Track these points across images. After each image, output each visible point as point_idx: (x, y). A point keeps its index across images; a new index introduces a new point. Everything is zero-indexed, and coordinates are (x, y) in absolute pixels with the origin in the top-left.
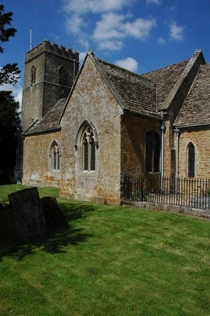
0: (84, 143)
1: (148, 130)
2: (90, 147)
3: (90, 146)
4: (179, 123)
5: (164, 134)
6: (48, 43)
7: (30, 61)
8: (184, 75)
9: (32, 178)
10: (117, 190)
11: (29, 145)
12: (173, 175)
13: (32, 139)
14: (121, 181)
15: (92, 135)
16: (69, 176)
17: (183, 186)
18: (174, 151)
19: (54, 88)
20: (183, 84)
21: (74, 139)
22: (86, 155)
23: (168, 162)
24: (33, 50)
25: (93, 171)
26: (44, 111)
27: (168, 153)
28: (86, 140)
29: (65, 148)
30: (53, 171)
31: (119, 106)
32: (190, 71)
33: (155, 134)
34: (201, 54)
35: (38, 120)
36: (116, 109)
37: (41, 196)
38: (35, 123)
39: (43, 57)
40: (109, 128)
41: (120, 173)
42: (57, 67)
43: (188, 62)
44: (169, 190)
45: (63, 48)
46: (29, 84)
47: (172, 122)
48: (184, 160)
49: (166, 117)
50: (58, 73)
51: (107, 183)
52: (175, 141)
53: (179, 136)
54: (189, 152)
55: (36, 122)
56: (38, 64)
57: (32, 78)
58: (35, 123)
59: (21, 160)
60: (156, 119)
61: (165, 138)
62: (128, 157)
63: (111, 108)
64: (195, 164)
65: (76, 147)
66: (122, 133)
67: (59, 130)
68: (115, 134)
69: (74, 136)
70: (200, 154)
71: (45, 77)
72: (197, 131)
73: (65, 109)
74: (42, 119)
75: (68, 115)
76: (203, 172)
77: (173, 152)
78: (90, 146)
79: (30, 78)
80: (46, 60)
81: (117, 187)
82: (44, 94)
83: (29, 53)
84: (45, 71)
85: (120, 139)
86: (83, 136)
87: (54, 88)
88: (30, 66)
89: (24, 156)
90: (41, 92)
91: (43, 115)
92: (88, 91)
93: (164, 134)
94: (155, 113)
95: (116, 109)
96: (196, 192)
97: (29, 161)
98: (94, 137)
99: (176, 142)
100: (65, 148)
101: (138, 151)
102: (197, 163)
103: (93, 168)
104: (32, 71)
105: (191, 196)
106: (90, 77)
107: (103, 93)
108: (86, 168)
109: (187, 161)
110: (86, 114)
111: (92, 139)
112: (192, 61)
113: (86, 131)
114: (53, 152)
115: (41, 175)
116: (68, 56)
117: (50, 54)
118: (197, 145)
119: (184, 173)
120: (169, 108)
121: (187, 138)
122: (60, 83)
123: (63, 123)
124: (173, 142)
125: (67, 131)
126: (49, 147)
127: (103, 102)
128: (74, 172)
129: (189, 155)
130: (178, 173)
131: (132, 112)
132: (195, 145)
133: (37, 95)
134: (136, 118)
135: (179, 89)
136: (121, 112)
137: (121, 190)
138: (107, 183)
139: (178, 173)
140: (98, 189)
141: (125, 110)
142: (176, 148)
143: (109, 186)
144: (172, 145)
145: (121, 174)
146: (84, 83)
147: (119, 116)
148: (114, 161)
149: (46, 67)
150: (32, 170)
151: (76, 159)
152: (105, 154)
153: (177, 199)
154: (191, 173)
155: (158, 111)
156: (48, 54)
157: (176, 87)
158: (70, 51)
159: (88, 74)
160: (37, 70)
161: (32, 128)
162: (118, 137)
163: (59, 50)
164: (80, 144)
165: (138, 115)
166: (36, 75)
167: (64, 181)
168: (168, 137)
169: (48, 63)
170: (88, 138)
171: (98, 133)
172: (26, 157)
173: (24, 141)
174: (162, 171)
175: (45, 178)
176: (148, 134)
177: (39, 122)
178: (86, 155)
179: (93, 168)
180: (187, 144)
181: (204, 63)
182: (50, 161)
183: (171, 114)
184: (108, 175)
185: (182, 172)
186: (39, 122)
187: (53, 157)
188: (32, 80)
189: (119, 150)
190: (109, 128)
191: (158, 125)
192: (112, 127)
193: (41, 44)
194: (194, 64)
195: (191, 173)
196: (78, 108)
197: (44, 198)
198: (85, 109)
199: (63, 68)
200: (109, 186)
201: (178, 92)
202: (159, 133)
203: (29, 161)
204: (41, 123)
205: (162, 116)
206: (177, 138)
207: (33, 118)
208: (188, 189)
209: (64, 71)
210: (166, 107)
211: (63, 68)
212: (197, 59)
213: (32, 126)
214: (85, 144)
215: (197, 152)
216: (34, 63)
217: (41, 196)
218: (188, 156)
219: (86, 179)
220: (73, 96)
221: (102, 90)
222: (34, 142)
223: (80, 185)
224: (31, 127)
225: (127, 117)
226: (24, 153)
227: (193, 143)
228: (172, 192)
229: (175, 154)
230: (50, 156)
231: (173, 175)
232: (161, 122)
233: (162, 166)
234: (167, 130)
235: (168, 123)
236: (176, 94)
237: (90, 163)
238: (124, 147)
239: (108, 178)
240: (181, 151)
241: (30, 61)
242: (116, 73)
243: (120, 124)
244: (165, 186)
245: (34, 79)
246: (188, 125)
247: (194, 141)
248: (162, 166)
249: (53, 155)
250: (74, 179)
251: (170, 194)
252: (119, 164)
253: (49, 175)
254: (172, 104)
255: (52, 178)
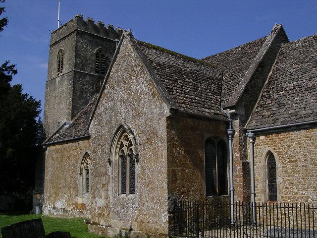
0: (121, 156)
1: (207, 136)
2: (129, 160)
3: (128, 160)
4: (252, 124)
5: (232, 140)
6: (80, 18)
7: (56, 43)
8: (259, 58)
9: (56, 206)
10: (164, 221)
11: (52, 155)
12: (247, 198)
13: (57, 151)
14: (169, 209)
15: (130, 145)
16: (101, 202)
17: (261, 214)
18: (248, 163)
19: (88, 78)
20: (257, 70)
21: (107, 150)
22: (124, 173)
23: (239, 180)
24: (61, 28)
25: (132, 196)
26: (74, 113)
27: (239, 167)
28: (123, 151)
29: (96, 164)
30: (84, 196)
31: (164, 105)
32: (266, 53)
33: (220, 141)
34: (282, 29)
35: (65, 124)
36: (161, 108)
37: (48, 231)
38: (61, 128)
39: (74, 36)
40: (152, 135)
41: (167, 197)
42: (93, 49)
43: (265, 40)
44: (242, 221)
45: (102, 25)
46: (54, 74)
47: (243, 123)
48: (262, 176)
49: (234, 116)
50: (94, 58)
51: (151, 211)
52: (249, 151)
53: (253, 143)
54: (268, 165)
55: (63, 126)
56: (68, 47)
57: (59, 65)
58: (61, 128)
59: (42, 179)
60: (219, 121)
61: (233, 145)
62: (179, 174)
63: (153, 107)
64: (278, 181)
65: (110, 161)
66: (168, 142)
67: (88, 138)
68: (159, 143)
69: (107, 147)
70: (283, 167)
71: (76, 65)
72: (277, 133)
73: (95, 109)
74: (72, 122)
75: (99, 118)
76: (289, 193)
77: (246, 166)
78: (128, 160)
79: (56, 66)
80: (77, 41)
81: (165, 217)
82: (74, 88)
83: (55, 32)
84: (77, 56)
85: (166, 151)
86: (119, 147)
87: (88, 78)
88: (56, 49)
89: (46, 175)
90: (69, 85)
91: (73, 117)
92: (125, 84)
93: (232, 140)
94: (218, 112)
95: (161, 108)
96: (280, 221)
97: (52, 182)
98: (133, 147)
99: (250, 151)
100: (96, 164)
101: (196, 163)
102: (279, 180)
103: (132, 191)
104: (59, 57)
105: (303, 223)
106: (127, 65)
107: (143, 87)
108: (123, 192)
109: (266, 178)
110: (124, 115)
111: (131, 150)
112: (270, 39)
113: (122, 139)
114: (84, 168)
115: (69, 201)
116: (108, 35)
117: (83, 33)
118: (278, 155)
119: (263, 195)
120: (237, 104)
121: (263, 145)
122: (97, 72)
123: (93, 128)
124: (246, 151)
125: (98, 140)
126: (80, 161)
127: (144, 100)
128: (107, 198)
129: (269, 169)
130: (255, 194)
131: (183, 113)
132: (275, 155)
133: (64, 89)
134: (189, 120)
135: (252, 78)
136: (167, 112)
137: (169, 222)
138: (151, 211)
139: (255, 194)
140: (139, 220)
141: (171, 110)
142: (250, 160)
143: (154, 216)
144: (244, 156)
145: (169, 198)
146: (119, 74)
147: (165, 118)
148: (159, 181)
149: (77, 50)
150: (57, 194)
151: (109, 178)
152: (147, 171)
153: (244, 232)
154: (273, 196)
155: (224, 109)
156: (80, 34)
157: (248, 74)
158: (111, 28)
159: (125, 61)
160: (66, 55)
161: (58, 135)
162: (163, 148)
163: (95, 28)
164: (115, 157)
165: (192, 116)
166: (64, 62)
167: (95, 210)
168: (238, 146)
169: (80, 45)
170: (125, 149)
171: (138, 143)
172: (48, 177)
173: (47, 153)
174: (232, 192)
175: (74, 206)
176: (209, 141)
177: (67, 126)
178: (124, 173)
179: (132, 191)
180: (265, 154)
181: (286, 40)
182: (81, 180)
183: (242, 112)
184: (152, 200)
185: (260, 196)
186: (67, 126)
187: (85, 174)
188: (59, 69)
189: (165, 164)
190: (152, 135)
191: (223, 128)
192: (156, 133)
193: (72, 21)
194: (273, 43)
195: (273, 196)
196: (112, 109)
197: (52, 234)
198: (121, 109)
199: (100, 51)
200: (154, 216)
201: (250, 81)
202: (225, 139)
203: (52, 182)
204: (70, 127)
205: (229, 115)
206: (251, 144)
207: (59, 121)
208: (269, 216)
209: (103, 55)
210: (234, 103)
211: (100, 51)
212: (277, 37)
213: (58, 131)
214: (122, 157)
215: (279, 165)
216: (62, 46)
217: (48, 231)
218: (267, 170)
219: (123, 207)
220: (105, 91)
221: (143, 84)
222: (59, 155)
223: (116, 216)
224: (55, 134)
225: (176, 119)
226: (46, 170)
227: (273, 151)
228: (249, 220)
229: (249, 169)
230: (81, 174)
231: (247, 198)
232: (227, 124)
233: (232, 188)
234: (236, 134)
235: (237, 122)
236: (248, 85)
237: (127, 184)
238: (171, 160)
239: (151, 205)
240: (257, 165)
241: (56, 43)
242: (163, 59)
243: (165, 129)
244: (234, 214)
245: (62, 67)
246: (265, 127)
247: (274, 149)
248: (232, 188)
249: (84, 172)
250: (107, 207)
251: (243, 225)
252: (165, 185)
253: (80, 201)
254: (240, 100)
255: (83, 206)
